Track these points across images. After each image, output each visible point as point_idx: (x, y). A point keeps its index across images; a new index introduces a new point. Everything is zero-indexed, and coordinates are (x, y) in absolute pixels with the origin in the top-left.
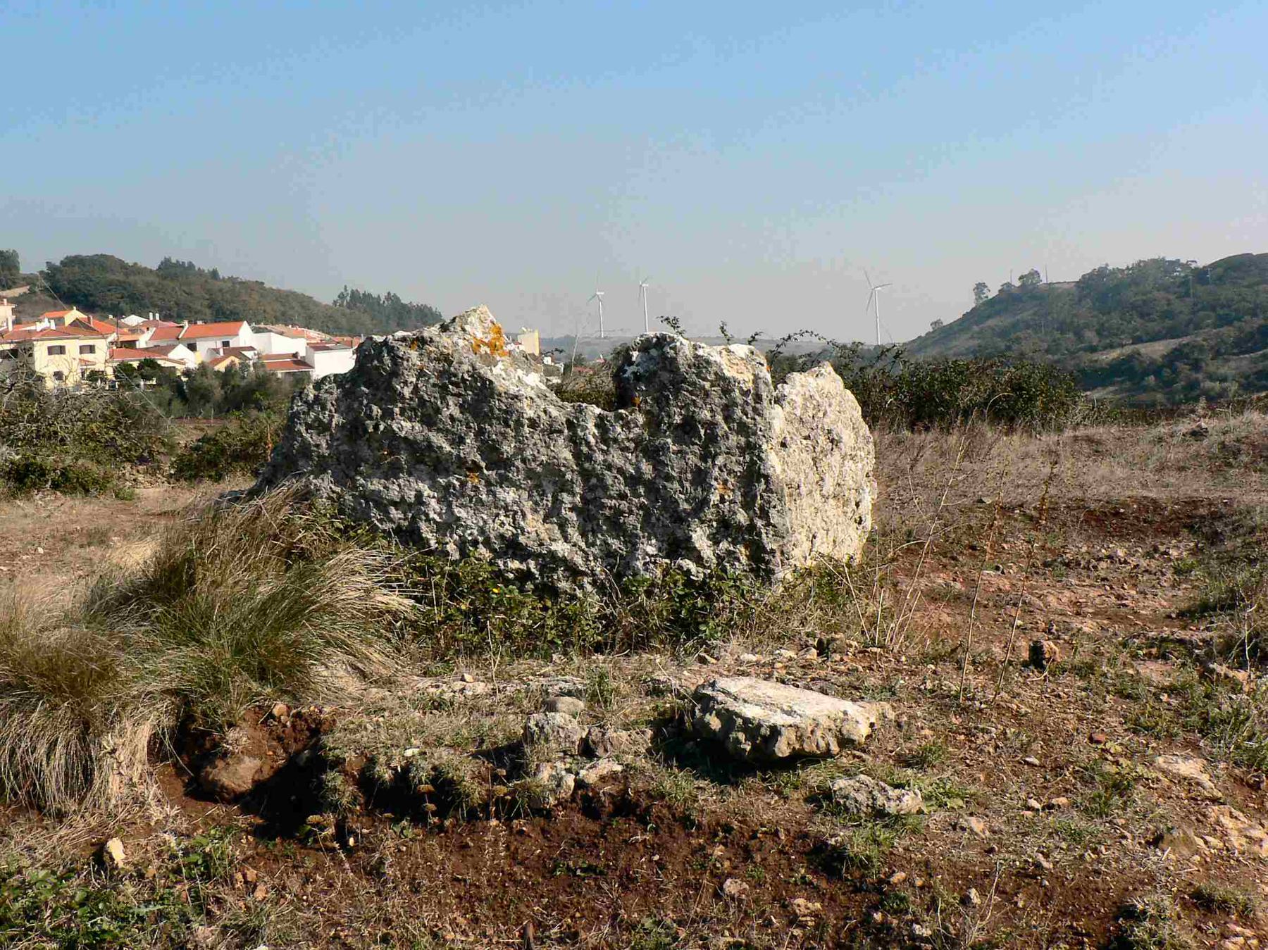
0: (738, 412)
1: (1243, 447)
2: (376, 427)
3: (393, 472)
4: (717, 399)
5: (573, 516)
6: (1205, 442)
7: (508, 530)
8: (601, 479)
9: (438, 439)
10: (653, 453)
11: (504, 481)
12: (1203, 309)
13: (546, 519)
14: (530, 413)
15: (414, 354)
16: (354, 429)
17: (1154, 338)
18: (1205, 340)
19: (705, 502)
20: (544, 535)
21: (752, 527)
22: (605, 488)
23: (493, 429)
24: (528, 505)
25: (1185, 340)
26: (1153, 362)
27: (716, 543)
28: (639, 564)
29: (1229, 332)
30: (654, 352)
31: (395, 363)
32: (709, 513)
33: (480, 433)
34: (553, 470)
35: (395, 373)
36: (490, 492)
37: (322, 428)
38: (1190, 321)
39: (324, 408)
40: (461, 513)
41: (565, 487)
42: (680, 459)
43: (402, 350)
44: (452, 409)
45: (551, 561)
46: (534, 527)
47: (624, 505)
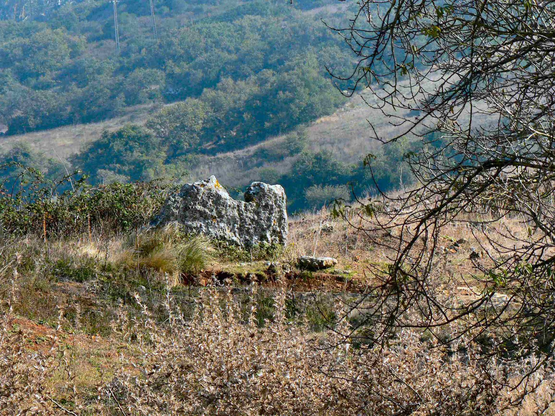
0: (278, 202)
1: (358, 236)
2: (192, 207)
3: (195, 219)
4: (273, 199)
5: (237, 230)
6: (332, 235)
7: (222, 234)
8: (245, 220)
9: (207, 210)
10: (257, 213)
11: (221, 221)
12: (140, 64)
13: (231, 231)
14: (229, 203)
15: (202, 188)
16: (186, 208)
17: (51, 121)
18: (150, 125)
19: (270, 225)
20: (231, 235)
21: (280, 232)
22: (246, 222)
23: (220, 207)
24: (226, 227)
25: (113, 126)
26: (54, 170)
27: (272, 236)
28: (254, 242)
29: (197, 111)
30: (257, 187)
31: (198, 191)
32: (271, 229)
33: (217, 209)
34: (234, 218)
35: (198, 193)
36: (218, 224)
37: (177, 208)
38: (116, 90)
39: (178, 203)
40: (210, 230)
41: (235, 222)
42: (264, 215)
43: (199, 188)
44: (210, 203)
45: (232, 242)
46: (229, 234)
47: (250, 227)
